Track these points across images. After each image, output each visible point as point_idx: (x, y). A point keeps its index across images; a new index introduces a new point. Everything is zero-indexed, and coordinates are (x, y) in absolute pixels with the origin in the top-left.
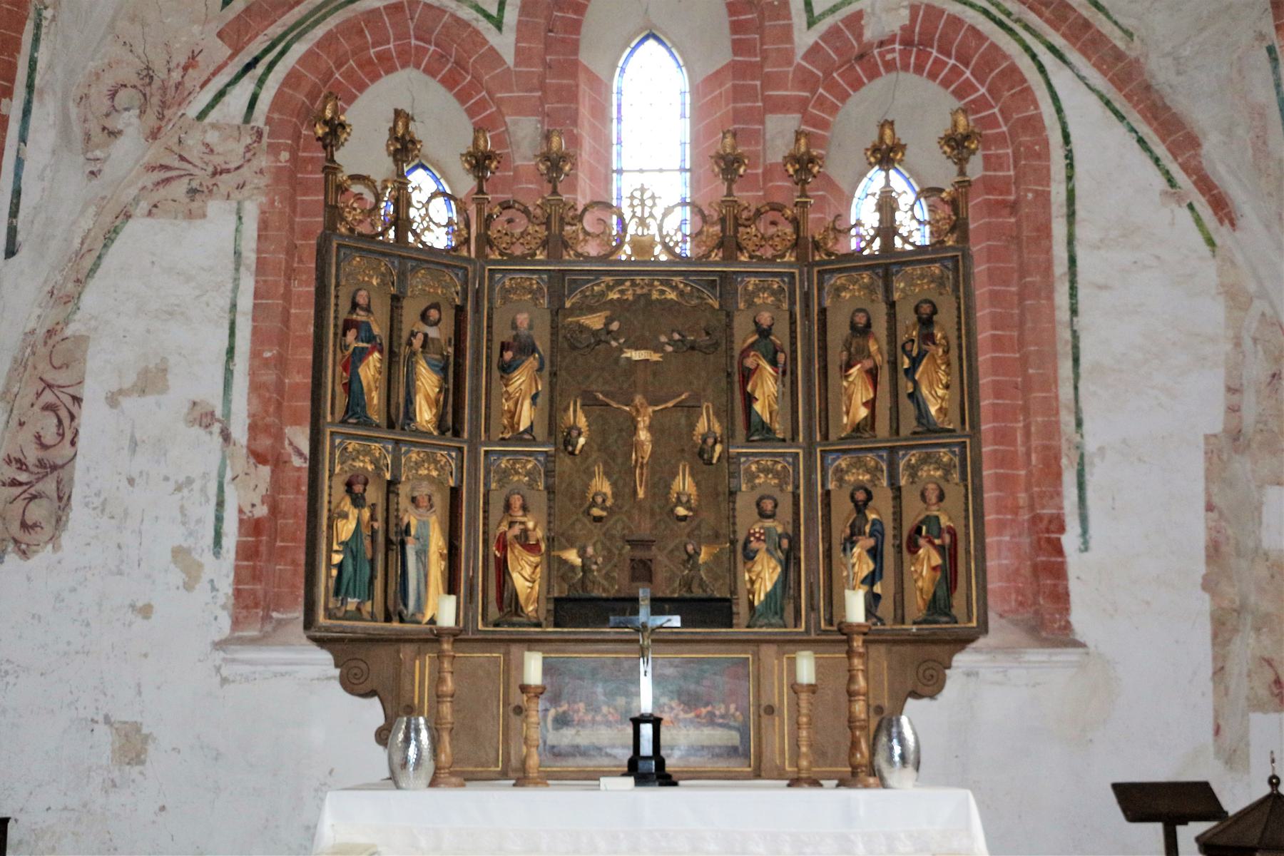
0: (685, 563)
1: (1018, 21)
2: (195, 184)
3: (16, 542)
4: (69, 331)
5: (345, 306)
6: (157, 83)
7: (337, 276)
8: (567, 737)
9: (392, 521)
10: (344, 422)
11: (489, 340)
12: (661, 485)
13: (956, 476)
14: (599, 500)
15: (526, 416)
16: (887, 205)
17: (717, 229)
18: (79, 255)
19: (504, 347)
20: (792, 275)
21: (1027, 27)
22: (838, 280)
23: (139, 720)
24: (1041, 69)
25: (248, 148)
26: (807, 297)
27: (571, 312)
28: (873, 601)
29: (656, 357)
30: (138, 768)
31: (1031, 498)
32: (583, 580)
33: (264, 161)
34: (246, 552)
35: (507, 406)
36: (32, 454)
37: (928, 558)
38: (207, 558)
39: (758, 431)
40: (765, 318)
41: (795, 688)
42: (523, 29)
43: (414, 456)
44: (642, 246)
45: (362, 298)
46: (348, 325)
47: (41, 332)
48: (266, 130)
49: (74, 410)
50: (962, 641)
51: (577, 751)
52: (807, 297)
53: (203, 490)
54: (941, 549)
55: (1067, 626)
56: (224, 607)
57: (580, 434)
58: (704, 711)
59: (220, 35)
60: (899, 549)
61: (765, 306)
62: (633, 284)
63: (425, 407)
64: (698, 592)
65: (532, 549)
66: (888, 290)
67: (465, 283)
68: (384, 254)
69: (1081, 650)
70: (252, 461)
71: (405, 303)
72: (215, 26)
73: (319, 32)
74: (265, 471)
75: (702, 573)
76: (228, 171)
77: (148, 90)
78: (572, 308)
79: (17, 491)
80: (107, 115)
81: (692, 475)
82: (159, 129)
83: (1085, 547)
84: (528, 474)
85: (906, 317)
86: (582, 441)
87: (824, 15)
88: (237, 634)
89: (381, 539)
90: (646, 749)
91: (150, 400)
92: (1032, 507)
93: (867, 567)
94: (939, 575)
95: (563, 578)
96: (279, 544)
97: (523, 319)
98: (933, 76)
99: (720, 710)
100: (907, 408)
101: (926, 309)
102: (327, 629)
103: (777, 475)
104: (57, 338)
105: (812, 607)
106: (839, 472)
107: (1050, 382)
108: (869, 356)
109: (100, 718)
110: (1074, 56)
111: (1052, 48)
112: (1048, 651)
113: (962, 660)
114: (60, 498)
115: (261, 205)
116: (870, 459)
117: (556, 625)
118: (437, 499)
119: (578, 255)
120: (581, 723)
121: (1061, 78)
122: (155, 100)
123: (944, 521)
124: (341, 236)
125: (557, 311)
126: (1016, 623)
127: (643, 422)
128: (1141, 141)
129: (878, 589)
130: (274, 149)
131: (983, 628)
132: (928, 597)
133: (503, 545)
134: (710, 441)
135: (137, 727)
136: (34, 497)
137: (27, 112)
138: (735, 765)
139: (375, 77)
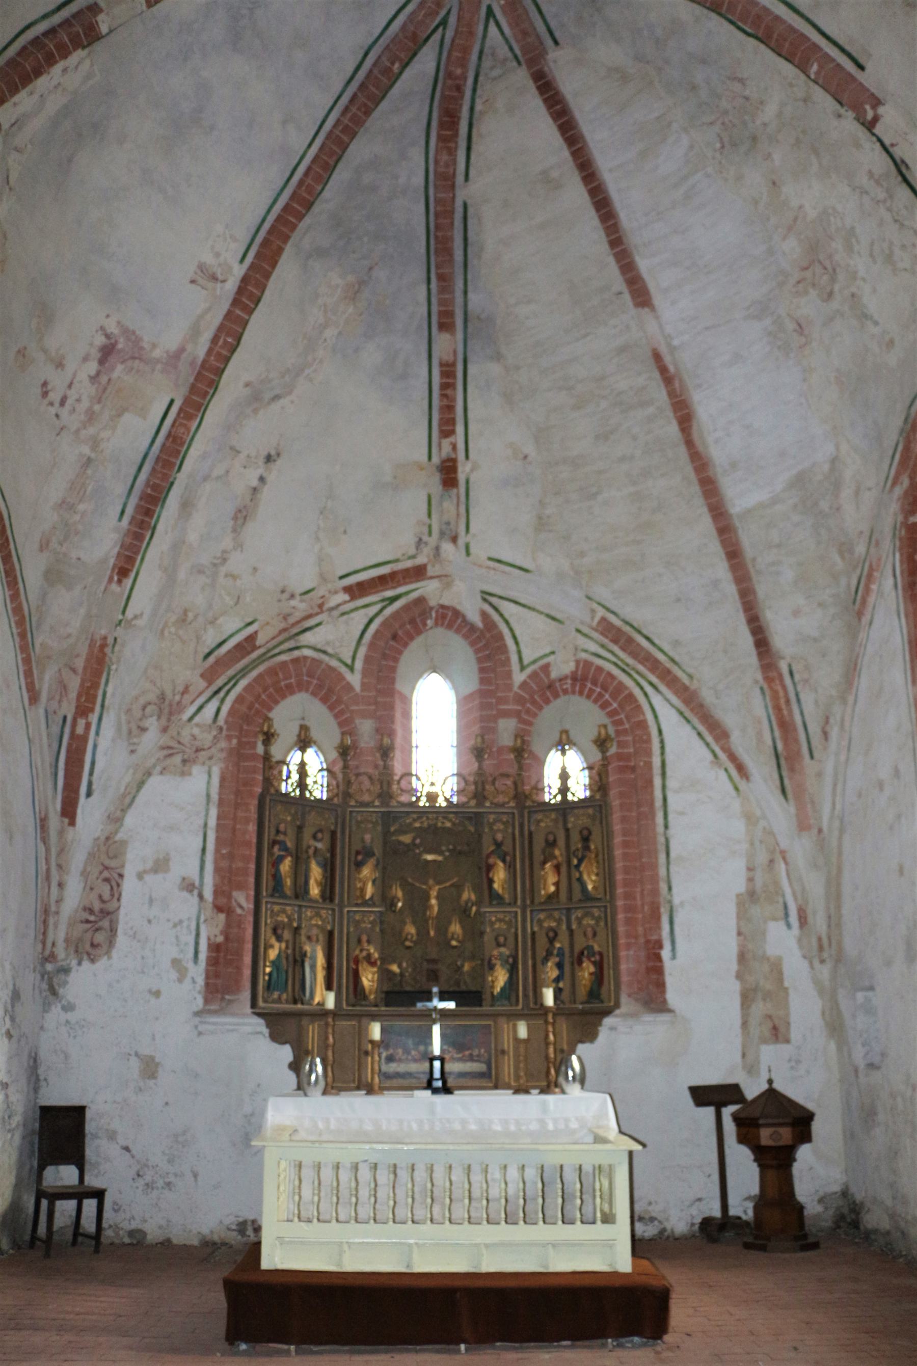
0: (456, 971)
1: (633, 669)
2: (186, 757)
3: (88, 954)
4: (117, 838)
5: (273, 831)
6: (167, 702)
7: (270, 815)
8: (393, 1067)
9: (297, 949)
10: (272, 896)
11: (350, 850)
12: (442, 930)
13: (602, 924)
14: (409, 937)
15: (369, 890)
16: (564, 776)
17: (473, 787)
18: (124, 796)
19: (358, 853)
20: (513, 814)
21: (638, 673)
22: (539, 816)
23: (153, 1054)
24: (646, 694)
25: (215, 737)
26: (521, 826)
27: (394, 833)
28: (558, 993)
29: (440, 858)
30: (154, 1081)
31: (645, 930)
32: (401, 981)
33: (223, 744)
34: (213, 962)
35: (359, 885)
36: (97, 906)
37: (587, 970)
38: (190, 965)
39: (495, 898)
40: (499, 837)
41: (517, 1040)
42: (365, 673)
43: (309, 914)
44: (432, 797)
45: (282, 827)
46: (275, 842)
47: (103, 838)
48: (225, 727)
49: (120, 881)
50: (607, 1012)
51: (398, 1075)
52: (521, 826)
53: (188, 927)
54: (594, 963)
55: (665, 1001)
56: (199, 992)
57: (399, 900)
58: (467, 1053)
59: (202, 676)
60: (572, 964)
61: (499, 830)
62: (428, 818)
63: (315, 887)
64: (463, 988)
65: (373, 964)
66: (565, 822)
67: (336, 819)
68: (294, 804)
69: (672, 1014)
70: (215, 911)
71: (305, 830)
72: (200, 671)
73: (254, 674)
74: (222, 917)
75: (466, 977)
76: (204, 750)
77: (162, 706)
78: (396, 831)
79: (89, 926)
80: (141, 720)
81: (460, 923)
82: (168, 727)
83: (674, 957)
84: (371, 923)
85: (575, 837)
86: (400, 904)
87: (529, 665)
88: (208, 1007)
89: (291, 959)
90: (437, 1074)
91: (160, 876)
92: (645, 935)
93: (555, 973)
94: (593, 977)
95: (390, 980)
96: (229, 957)
97: (368, 837)
98: (588, 697)
99: (476, 1052)
100: (576, 886)
101: (585, 833)
102: (264, 1008)
103: (506, 922)
104: (111, 842)
105: (526, 996)
106: (540, 922)
107: (654, 866)
108: (555, 857)
109: (133, 1053)
110: (662, 688)
111: (651, 684)
112: (654, 1015)
113: (608, 1021)
114: (111, 931)
115: (221, 768)
116: (556, 914)
117: (386, 1006)
118: (321, 938)
119: (398, 802)
120: (400, 1060)
121: (657, 700)
122: (166, 711)
123: (596, 948)
124: (272, 795)
125: (386, 833)
126: (637, 1000)
127: (434, 893)
128: (699, 734)
129: (561, 985)
130: (229, 738)
131: (617, 1005)
132: (588, 989)
133: (357, 961)
134: (470, 905)
135: (152, 1058)
136: (97, 930)
137: (100, 719)
138: (484, 1082)
139: (284, 697)
